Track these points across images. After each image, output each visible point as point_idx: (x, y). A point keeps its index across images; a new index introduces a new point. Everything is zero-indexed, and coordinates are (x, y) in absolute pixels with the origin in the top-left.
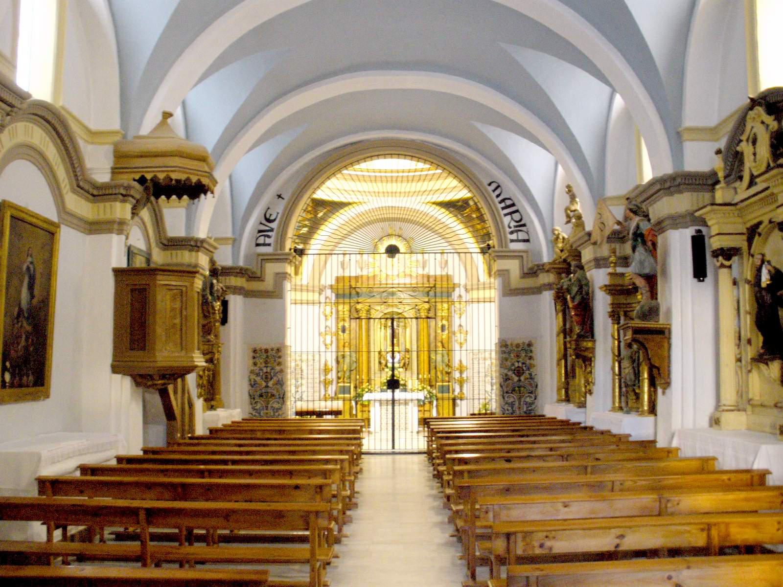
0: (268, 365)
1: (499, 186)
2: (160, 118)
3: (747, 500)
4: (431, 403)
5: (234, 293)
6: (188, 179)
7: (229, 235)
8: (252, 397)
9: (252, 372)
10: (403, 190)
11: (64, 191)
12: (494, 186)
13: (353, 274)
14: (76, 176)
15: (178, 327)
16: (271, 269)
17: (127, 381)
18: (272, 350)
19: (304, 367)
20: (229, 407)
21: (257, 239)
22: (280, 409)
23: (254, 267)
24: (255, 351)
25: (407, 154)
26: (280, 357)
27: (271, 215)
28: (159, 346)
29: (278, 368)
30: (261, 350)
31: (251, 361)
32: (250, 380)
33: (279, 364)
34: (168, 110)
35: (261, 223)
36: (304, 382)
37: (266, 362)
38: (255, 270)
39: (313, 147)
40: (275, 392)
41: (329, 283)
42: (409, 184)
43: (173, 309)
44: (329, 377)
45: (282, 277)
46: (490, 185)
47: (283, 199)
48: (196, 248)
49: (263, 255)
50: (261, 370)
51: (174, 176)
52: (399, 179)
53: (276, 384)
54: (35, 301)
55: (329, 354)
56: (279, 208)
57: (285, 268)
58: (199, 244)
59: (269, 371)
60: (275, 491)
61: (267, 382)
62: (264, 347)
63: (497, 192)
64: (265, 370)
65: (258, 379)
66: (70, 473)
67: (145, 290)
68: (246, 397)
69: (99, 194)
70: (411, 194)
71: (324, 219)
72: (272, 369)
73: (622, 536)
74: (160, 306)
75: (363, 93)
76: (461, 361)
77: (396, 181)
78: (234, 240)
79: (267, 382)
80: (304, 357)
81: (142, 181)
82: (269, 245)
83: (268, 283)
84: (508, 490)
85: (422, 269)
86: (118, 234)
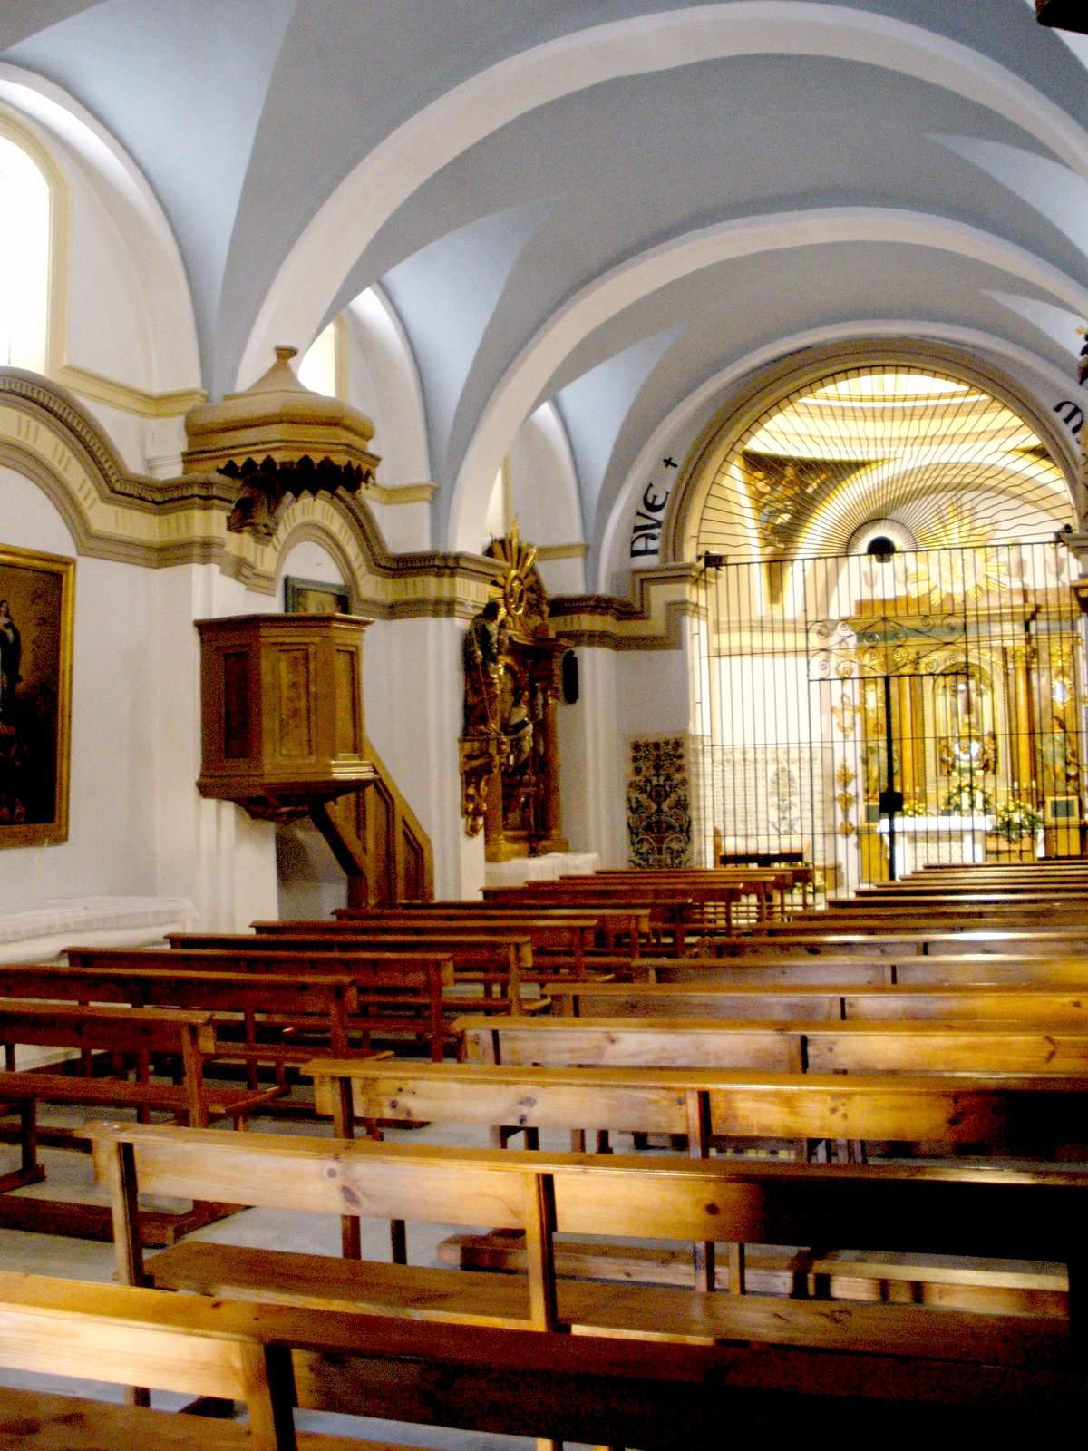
0: (661, 773)
1: (1076, 410)
2: (272, 359)
3: (973, 1048)
4: (1033, 835)
5: (591, 644)
6: (306, 460)
7: (576, 537)
8: (633, 831)
9: (631, 785)
10: (895, 435)
11: (85, 505)
12: (1067, 410)
13: (889, 595)
14: (105, 476)
15: (304, 712)
16: (659, 596)
17: (229, 810)
18: (667, 743)
19: (794, 769)
20: (577, 851)
21: (633, 543)
22: (682, 851)
23: (628, 594)
24: (636, 747)
25: (887, 362)
26: (680, 757)
27: (655, 497)
28: (267, 749)
29: (677, 777)
30: (647, 745)
31: (630, 767)
32: (629, 800)
33: (680, 769)
35: (639, 514)
36: (795, 800)
37: (657, 767)
38: (628, 599)
39: (716, 367)
40: (673, 821)
41: (845, 613)
42: (906, 423)
43: (294, 685)
44: (851, 790)
45: (678, 610)
46: (1058, 409)
47: (675, 466)
48: (448, 571)
49: (640, 571)
50: (648, 780)
51: (278, 457)
52: (887, 414)
53: (676, 807)
54: (21, 687)
55: (850, 746)
56: (667, 483)
57: (684, 591)
58: (451, 563)
59: (662, 783)
61: (659, 804)
62: (652, 740)
63: (1075, 422)
64: (655, 781)
65: (643, 797)
66: (52, 961)
67: (245, 654)
68: (623, 831)
69: (164, 498)
70: (910, 442)
71: (822, 493)
72: (668, 778)
73: (529, 1102)
74: (267, 680)
75: (794, 253)
76: (845, 767)
77: (912, 415)
78: (586, 549)
79: (659, 804)
80: (794, 755)
81: (230, 470)
82: (654, 552)
83: (656, 623)
85: (1054, 578)
86: (204, 563)
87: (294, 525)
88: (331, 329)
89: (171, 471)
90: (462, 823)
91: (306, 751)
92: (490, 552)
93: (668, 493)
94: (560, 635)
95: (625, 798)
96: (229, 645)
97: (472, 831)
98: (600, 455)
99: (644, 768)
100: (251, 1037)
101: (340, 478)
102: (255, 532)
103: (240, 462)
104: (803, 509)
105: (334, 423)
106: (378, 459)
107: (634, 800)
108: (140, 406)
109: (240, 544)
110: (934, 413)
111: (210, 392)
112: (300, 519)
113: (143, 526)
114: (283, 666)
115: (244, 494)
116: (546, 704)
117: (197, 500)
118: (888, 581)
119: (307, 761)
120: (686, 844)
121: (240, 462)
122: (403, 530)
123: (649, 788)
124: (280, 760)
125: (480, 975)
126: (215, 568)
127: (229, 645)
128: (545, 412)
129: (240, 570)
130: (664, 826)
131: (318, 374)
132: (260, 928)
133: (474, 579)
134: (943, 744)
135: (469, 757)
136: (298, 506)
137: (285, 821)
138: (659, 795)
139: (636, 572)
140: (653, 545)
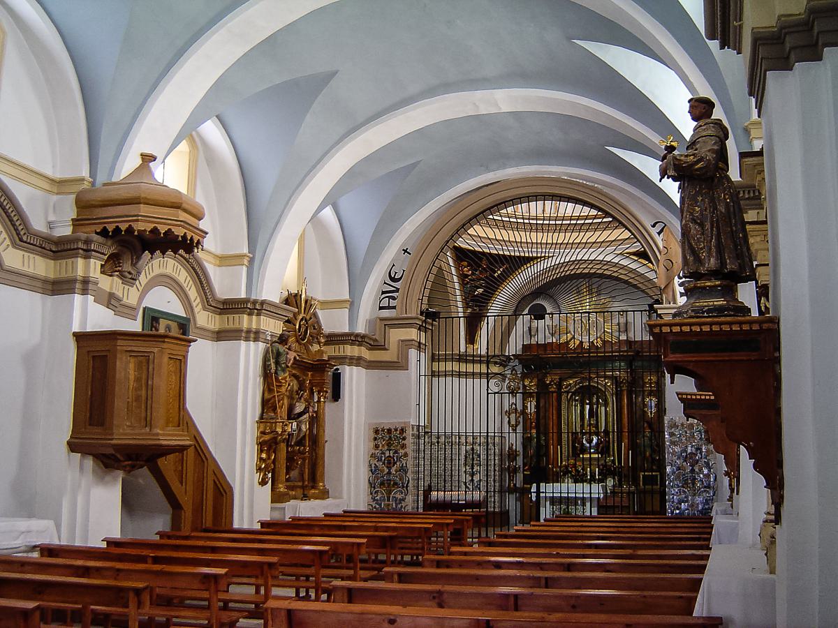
7: (347, 297)
8: (372, 485)
9: (373, 456)
11: (196, 310)
21: (380, 302)
24: (377, 432)
27: (396, 273)
29: (402, 452)
31: (372, 444)
34: (147, 151)
37: (389, 445)
46: (654, 226)
58: (258, 307)
59: (392, 455)
60: (30, 567)
61: (389, 468)
69: (58, 249)
72: (396, 452)
74: (120, 375)
79: (389, 468)
81: (104, 233)
82: (394, 308)
84: (477, 579)
87: (152, 275)
88: (184, 146)
89: (65, 231)
90: (257, 477)
91: (143, 423)
92: (287, 301)
93: (404, 271)
94: (330, 358)
95: (367, 464)
96: (96, 352)
97: (263, 483)
98: (362, 242)
99: (381, 446)
100: (69, 620)
101: (183, 246)
102: (122, 276)
103: (111, 228)
104: (492, 287)
105: (177, 206)
106: (207, 233)
107: (373, 466)
108: (47, 186)
109: (108, 283)
110: (581, 228)
111: (95, 180)
112: (157, 271)
113: (40, 266)
114: (132, 366)
115: (112, 250)
116: (319, 401)
117: (81, 251)
118: (543, 332)
119: (143, 431)
120: (406, 495)
121: (111, 228)
122: (228, 283)
123: (383, 458)
124: (125, 432)
125: (253, 580)
126: (91, 298)
127: (96, 352)
128: (328, 213)
129: (111, 301)
130: (392, 483)
131: (172, 175)
132: (110, 543)
133: (273, 317)
134: (575, 438)
135: (263, 433)
136: (155, 262)
137: (129, 470)
138: (389, 463)
139: (382, 319)
140: (393, 303)
